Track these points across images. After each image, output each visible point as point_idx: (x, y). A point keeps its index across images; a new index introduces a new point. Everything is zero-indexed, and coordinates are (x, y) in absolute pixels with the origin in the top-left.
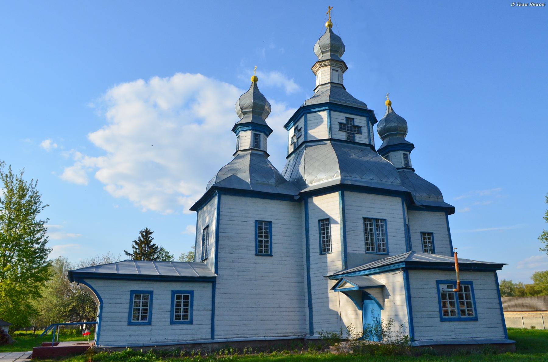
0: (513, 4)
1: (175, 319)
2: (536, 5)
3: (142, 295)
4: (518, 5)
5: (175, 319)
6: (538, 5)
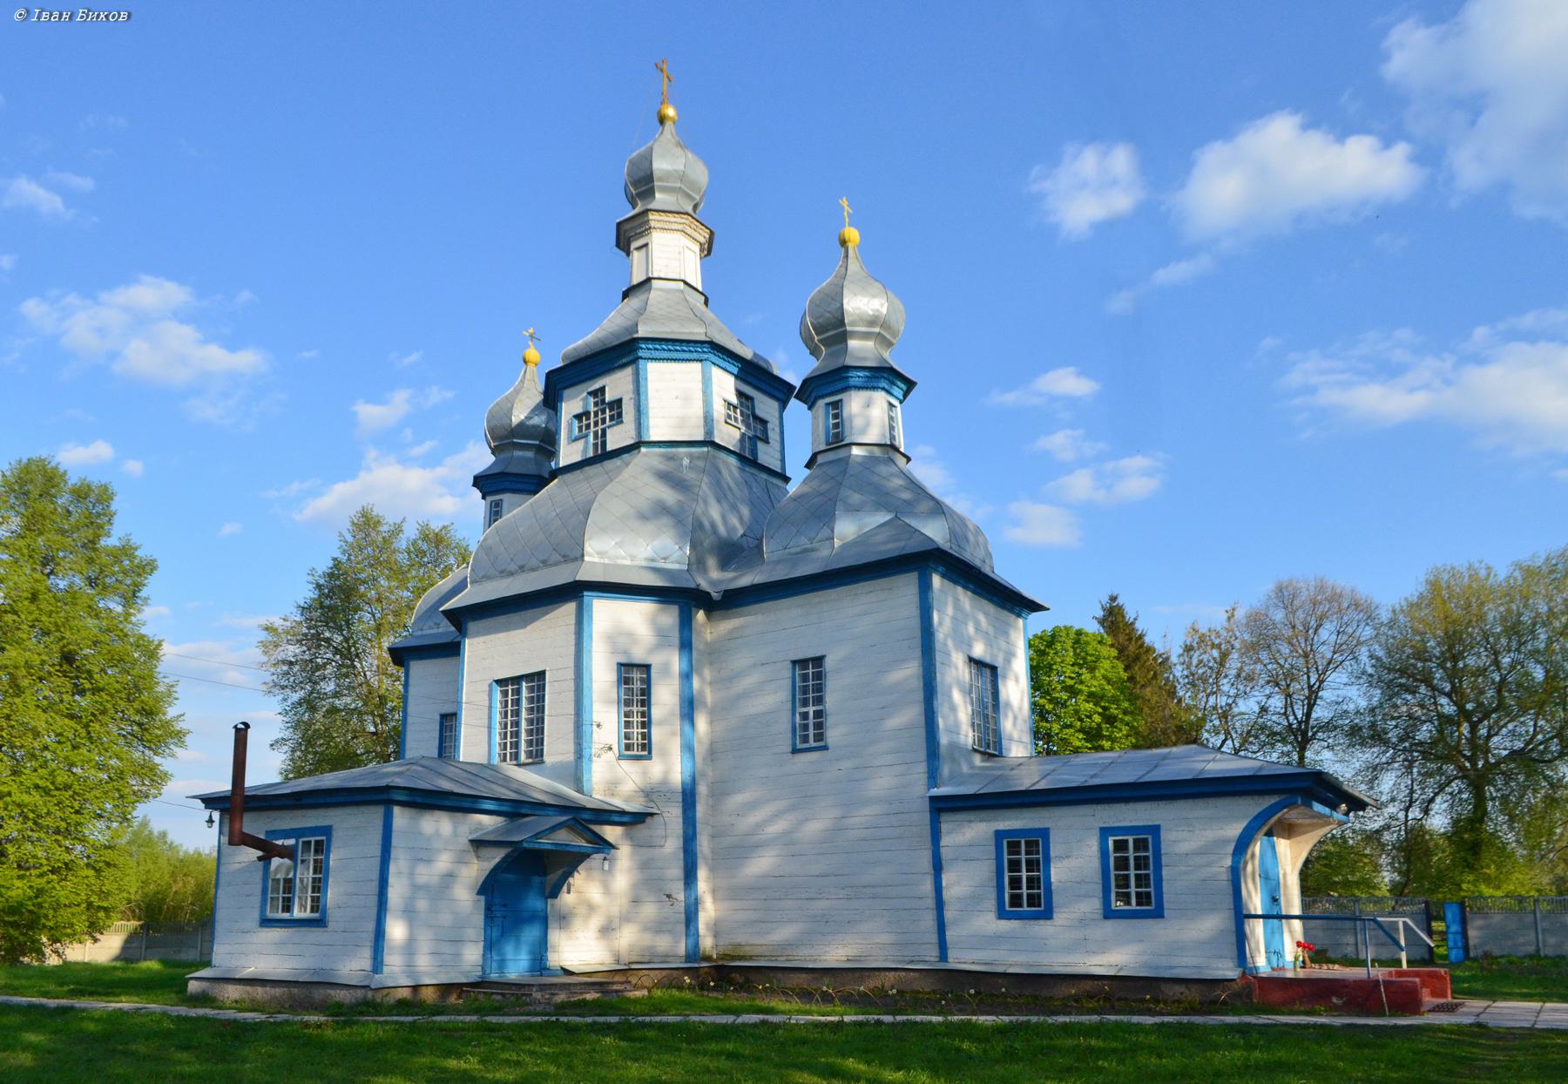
0: (20, 15)
1: (1039, 906)
2: (98, 16)
3: (1405, 965)
4: (39, 18)
5: (1039, 906)
6: (107, 17)
